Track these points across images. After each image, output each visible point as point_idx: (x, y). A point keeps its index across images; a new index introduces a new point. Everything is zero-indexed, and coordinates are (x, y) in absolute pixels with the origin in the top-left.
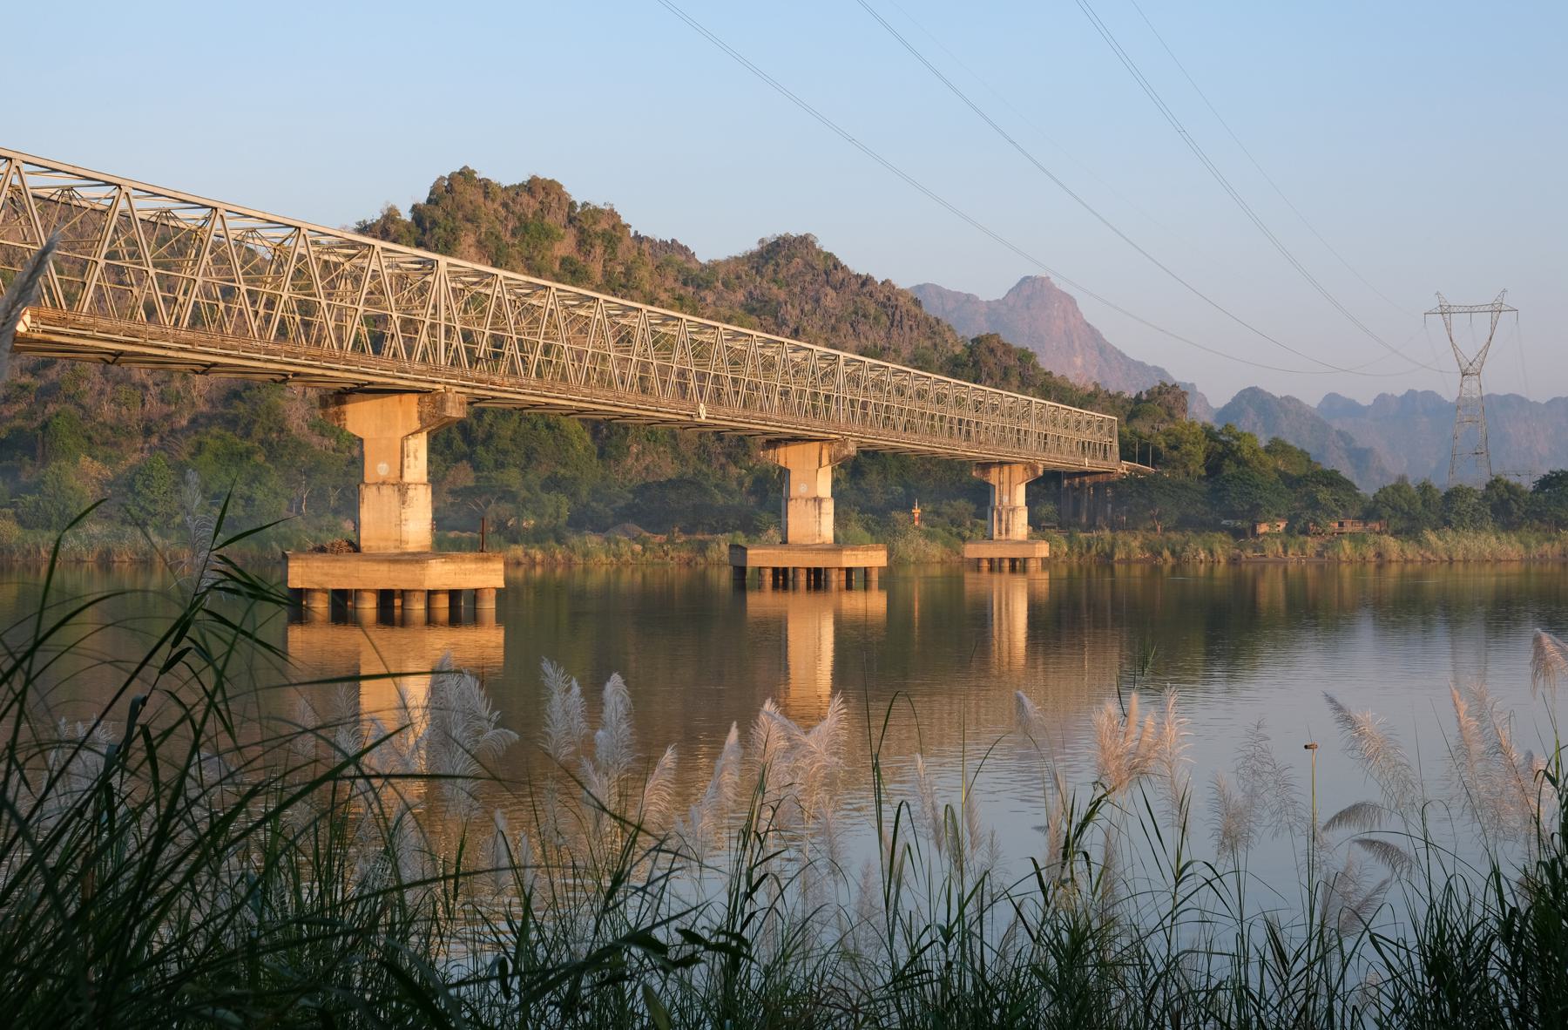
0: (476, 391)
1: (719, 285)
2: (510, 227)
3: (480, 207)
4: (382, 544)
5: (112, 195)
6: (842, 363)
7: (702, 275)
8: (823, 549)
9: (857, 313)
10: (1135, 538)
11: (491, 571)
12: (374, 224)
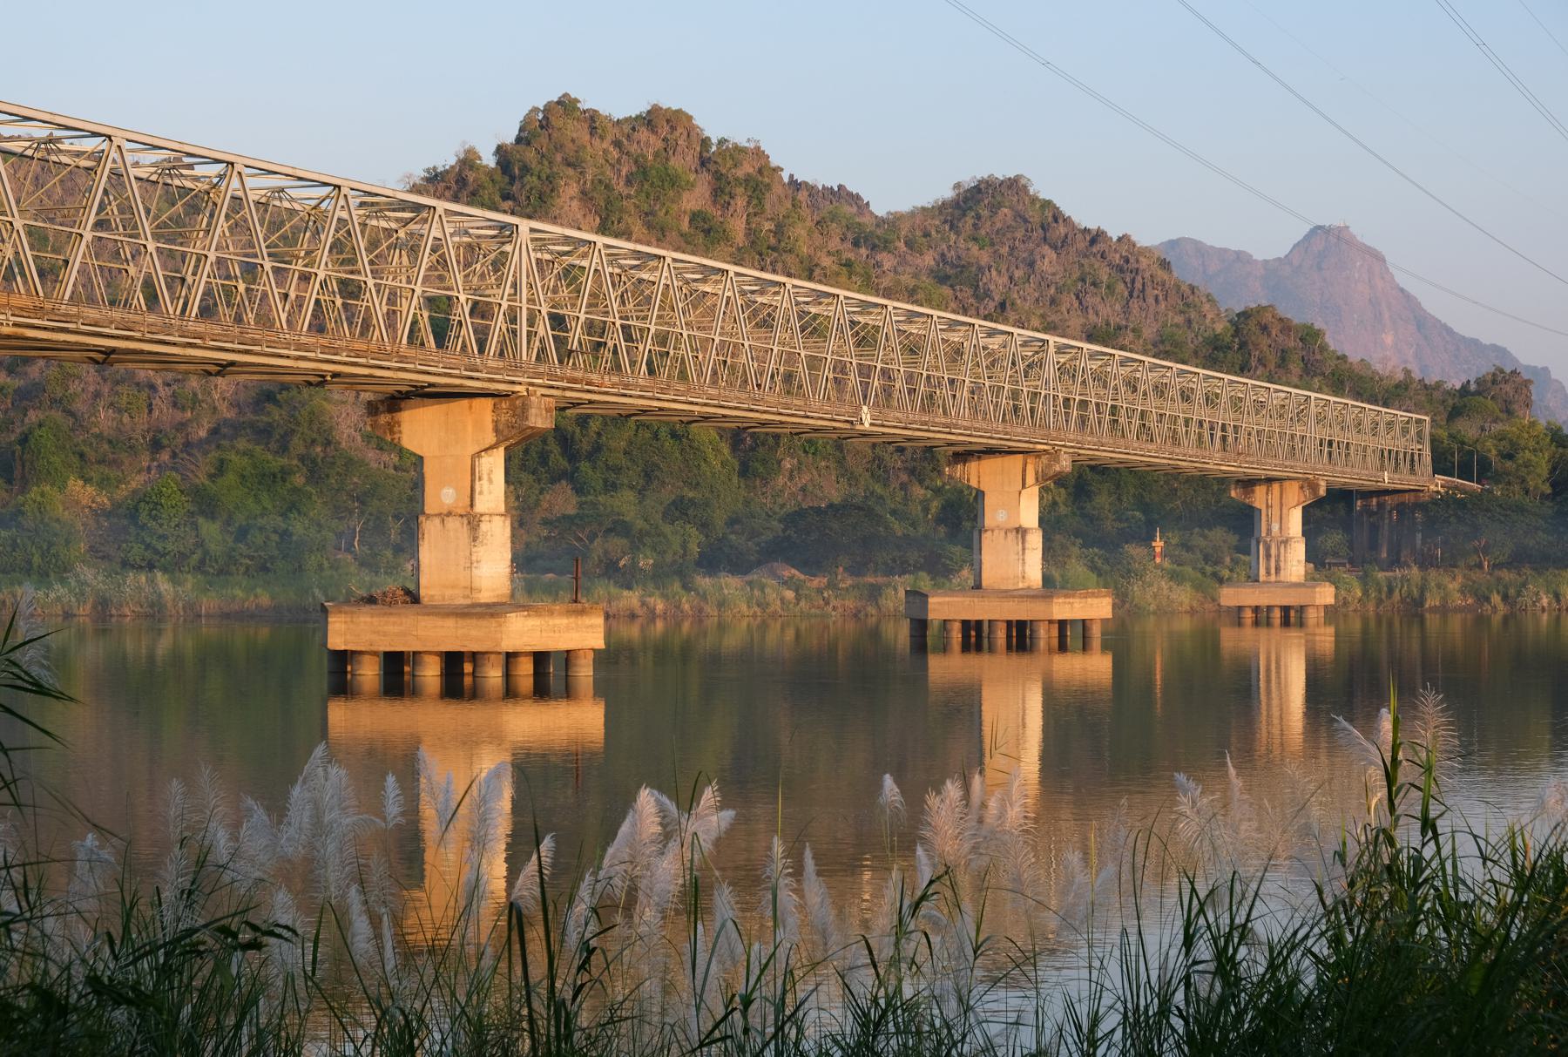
0: (568, 394)
1: (901, 245)
2: (624, 173)
3: (585, 147)
4: (449, 592)
5: (100, 148)
6: (1052, 350)
7: (879, 232)
8: (1028, 595)
9: (1083, 280)
10: (1454, 578)
11: (588, 627)
12: (447, 172)
